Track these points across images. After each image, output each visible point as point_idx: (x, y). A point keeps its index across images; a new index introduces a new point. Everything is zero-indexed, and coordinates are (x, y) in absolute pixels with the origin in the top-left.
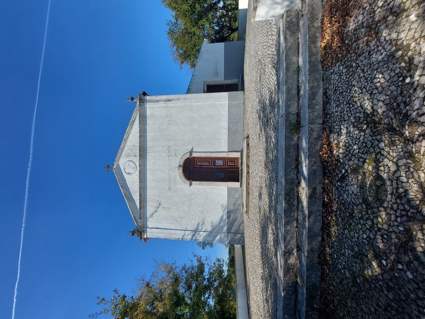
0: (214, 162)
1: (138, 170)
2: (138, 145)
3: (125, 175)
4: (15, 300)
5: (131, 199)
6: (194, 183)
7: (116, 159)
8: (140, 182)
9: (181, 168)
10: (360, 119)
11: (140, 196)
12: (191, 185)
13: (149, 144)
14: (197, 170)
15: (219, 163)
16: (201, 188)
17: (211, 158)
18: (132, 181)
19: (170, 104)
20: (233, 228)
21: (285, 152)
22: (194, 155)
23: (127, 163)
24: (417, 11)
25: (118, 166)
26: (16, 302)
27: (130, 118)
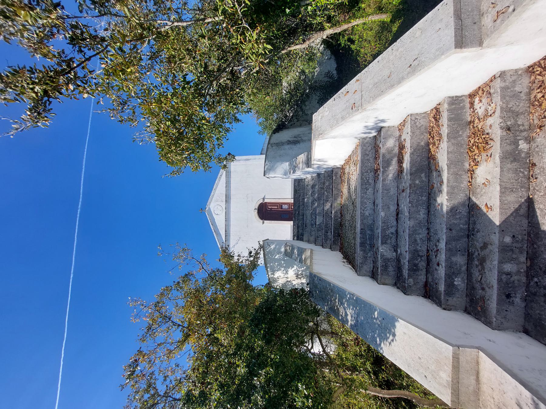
0: (281, 206)
1: (224, 212)
2: (224, 193)
3: (214, 216)
4: (62, 363)
5: (218, 234)
6: (265, 221)
7: (208, 204)
8: (226, 221)
9: (257, 211)
10: (272, 319)
11: (226, 231)
12: (263, 223)
13: (233, 192)
14: (266, 212)
15: (285, 207)
16: (270, 225)
17: (279, 203)
18: (220, 221)
19: (248, 163)
20: (409, 130)
21: (411, 140)
22: (266, 201)
23: (215, 207)
24: (383, 155)
25: (209, 208)
26: (63, 364)
27: (219, 173)
